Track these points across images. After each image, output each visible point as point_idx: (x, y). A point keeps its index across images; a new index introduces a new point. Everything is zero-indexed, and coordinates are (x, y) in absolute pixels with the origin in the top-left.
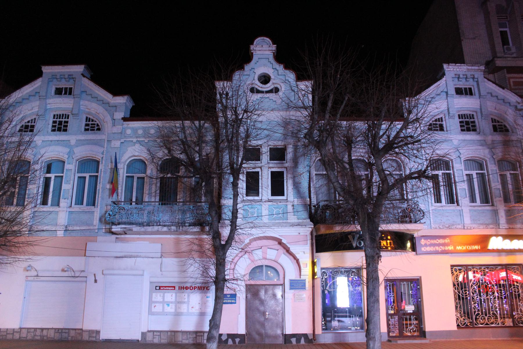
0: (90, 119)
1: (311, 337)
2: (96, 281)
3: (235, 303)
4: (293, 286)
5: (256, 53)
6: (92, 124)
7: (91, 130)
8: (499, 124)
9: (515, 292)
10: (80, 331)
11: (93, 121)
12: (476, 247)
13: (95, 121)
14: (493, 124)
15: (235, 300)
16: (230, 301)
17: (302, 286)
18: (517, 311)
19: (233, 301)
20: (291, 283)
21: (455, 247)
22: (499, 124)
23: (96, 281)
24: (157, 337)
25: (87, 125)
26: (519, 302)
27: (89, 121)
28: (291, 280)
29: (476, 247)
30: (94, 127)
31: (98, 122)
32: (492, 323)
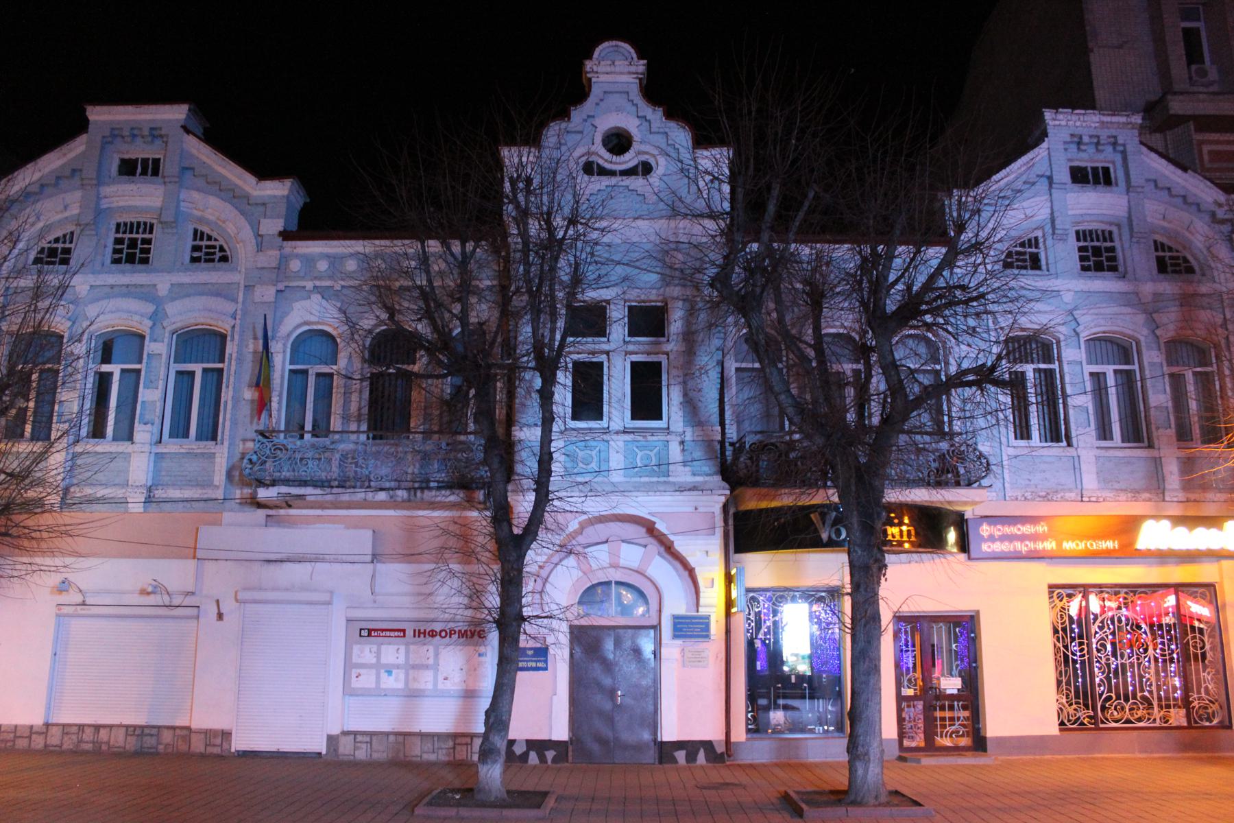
0: (202, 233)
1: (720, 749)
2: (220, 616)
3: (546, 669)
4: (681, 630)
5: (600, 80)
6: (208, 247)
7: (206, 261)
8: (1170, 254)
9: (1195, 647)
10: (185, 732)
11: (209, 238)
12: (1110, 544)
13: (216, 240)
14: (195, 243)
15: (546, 662)
16: (534, 664)
17: (702, 630)
18: (1199, 692)
19: (540, 665)
20: (675, 624)
21: (1059, 544)
22: (209, 243)
23: (220, 616)
24: (364, 746)
25: (196, 248)
26: (1204, 671)
27: (202, 239)
28: (675, 617)
29: (1110, 544)
30: (214, 253)
31: (222, 242)
32: (1140, 720)
